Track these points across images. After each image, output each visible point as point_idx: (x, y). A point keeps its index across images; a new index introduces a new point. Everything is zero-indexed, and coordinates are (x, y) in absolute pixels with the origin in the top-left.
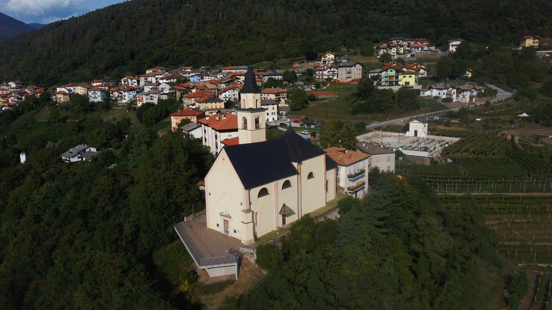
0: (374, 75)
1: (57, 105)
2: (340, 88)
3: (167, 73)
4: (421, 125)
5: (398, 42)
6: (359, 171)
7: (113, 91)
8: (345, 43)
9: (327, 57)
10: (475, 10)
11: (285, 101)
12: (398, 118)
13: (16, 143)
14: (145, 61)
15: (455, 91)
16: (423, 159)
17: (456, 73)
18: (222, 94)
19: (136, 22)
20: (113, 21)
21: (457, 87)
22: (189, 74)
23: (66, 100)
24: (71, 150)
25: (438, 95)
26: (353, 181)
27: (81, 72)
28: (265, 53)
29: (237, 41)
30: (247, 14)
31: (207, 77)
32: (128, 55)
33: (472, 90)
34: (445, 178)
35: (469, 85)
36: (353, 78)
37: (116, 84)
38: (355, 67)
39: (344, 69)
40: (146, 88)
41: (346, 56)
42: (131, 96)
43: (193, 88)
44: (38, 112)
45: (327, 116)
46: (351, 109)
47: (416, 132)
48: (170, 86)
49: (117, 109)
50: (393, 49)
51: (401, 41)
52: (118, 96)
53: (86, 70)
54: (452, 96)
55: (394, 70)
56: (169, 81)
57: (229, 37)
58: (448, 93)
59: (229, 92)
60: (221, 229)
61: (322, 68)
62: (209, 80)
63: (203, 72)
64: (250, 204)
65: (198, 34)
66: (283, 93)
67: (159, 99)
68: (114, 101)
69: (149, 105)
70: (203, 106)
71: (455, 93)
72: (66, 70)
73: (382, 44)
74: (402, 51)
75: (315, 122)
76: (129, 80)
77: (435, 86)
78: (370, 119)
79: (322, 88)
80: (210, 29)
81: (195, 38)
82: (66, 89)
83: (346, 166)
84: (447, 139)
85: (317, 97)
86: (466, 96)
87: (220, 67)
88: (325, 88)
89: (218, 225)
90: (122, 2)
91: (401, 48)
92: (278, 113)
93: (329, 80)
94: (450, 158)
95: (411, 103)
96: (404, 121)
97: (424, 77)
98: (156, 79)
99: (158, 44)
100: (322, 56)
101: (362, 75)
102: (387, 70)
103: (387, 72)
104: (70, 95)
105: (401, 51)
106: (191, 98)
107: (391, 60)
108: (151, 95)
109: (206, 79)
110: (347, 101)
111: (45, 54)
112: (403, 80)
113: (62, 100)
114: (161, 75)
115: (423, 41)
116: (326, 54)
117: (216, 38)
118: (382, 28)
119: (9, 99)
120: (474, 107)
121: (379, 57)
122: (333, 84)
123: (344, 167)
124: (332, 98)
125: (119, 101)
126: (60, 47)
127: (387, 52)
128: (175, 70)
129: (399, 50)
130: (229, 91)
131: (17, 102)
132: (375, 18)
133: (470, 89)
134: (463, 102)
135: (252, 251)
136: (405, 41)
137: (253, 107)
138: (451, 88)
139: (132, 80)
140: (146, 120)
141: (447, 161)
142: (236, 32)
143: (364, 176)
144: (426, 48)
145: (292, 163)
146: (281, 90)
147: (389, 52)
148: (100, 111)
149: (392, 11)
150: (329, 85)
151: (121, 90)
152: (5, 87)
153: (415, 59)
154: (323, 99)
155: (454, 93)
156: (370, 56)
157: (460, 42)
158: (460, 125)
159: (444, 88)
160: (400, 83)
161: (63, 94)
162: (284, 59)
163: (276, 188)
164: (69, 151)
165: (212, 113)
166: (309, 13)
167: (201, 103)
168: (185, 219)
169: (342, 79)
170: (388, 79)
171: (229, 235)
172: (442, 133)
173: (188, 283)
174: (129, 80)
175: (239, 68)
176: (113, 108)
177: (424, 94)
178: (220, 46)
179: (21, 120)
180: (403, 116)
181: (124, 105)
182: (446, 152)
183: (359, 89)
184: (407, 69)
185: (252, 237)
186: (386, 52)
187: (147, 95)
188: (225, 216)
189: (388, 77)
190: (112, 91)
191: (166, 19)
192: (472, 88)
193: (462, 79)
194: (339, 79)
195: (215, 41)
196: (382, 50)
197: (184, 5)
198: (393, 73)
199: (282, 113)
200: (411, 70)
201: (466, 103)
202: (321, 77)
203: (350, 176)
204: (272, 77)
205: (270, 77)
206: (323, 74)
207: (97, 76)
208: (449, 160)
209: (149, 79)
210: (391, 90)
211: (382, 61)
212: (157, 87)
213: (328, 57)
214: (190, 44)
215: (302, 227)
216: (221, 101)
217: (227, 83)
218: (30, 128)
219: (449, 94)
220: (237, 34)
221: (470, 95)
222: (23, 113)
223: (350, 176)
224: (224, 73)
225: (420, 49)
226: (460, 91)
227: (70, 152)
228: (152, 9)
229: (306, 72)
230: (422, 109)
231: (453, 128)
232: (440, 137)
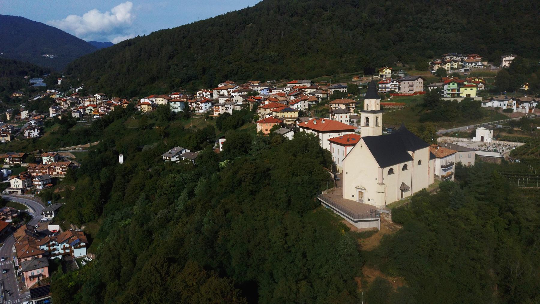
0: (434, 88)
1: (142, 114)
2: (404, 100)
3: (238, 87)
4: (487, 131)
5: (451, 58)
6: (449, 164)
7: (191, 103)
8: (401, 59)
9: (384, 72)
10: (527, 27)
11: (354, 110)
12: (463, 126)
13: (115, 146)
14: (217, 76)
15: (515, 102)
16: (494, 159)
17: (513, 87)
18: (295, 105)
19: (205, 41)
20: (184, 40)
21: (517, 99)
22: (257, 88)
23: (150, 110)
24: (170, 151)
25: (499, 106)
26: (445, 171)
27: (158, 85)
28: (325, 69)
29: (298, 57)
30: (306, 33)
31: (275, 91)
32: (201, 70)
33: (532, 102)
34: (516, 175)
35: (529, 97)
36: (415, 91)
37: (192, 96)
38: (417, 81)
39: (406, 82)
40: (221, 99)
41: (401, 70)
42: (207, 107)
43: (265, 99)
44: (126, 120)
45: (397, 123)
46: (418, 118)
47: (482, 138)
48: (244, 98)
49: (196, 118)
50: (447, 65)
51: (455, 57)
52: (196, 107)
53: (162, 83)
54: (513, 107)
55: (456, 83)
56: (240, 94)
57: (291, 55)
58: (508, 104)
59: (300, 103)
60: (356, 199)
61: (385, 81)
62: (277, 93)
63: (270, 86)
64: (383, 179)
65: (263, 51)
66: (353, 103)
67: (233, 110)
68: (192, 111)
69: (227, 114)
70: (280, 115)
71: (515, 104)
72: (145, 84)
73: (436, 60)
74: (456, 67)
75: (387, 129)
76: (204, 93)
77: (496, 97)
78: (437, 126)
79: (386, 99)
80: (274, 47)
81: (260, 55)
82: (149, 100)
83: (441, 158)
84: (512, 144)
85: (384, 107)
86: (525, 107)
87: (284, 82)
88: (389, 99)
89: (353, 196)
90: (190, 23)
91: (455, 63)
92: (350, 121)
93: (391, 92)
94: (518, 159)
95: (475, 113)
96: (469, 128)
97: (482, 90)
98: (229, 92)
99: (227, 60)
100: (380, 70)
101: (423, 88)
102: (449, 84)
103: (449, 86)
104: (152, 105)
105: (455, 66)
106: (267, 108)
107: (446, 75)
108: (226, 106)
109: (275, 92)
110: (413, 111)
111: (124, 70)
112: (465, 92)
113: (146, 110)
114: (233, 88)
115: (475, 56)
116: (384, 69)
117: (279, 55)
118: (435, 45)
119: (100, 109)
120: (535, 117)
121: (435, 72)
122: (397, 96)
123: (439, 159)
124: (399, 108)
125: (197, 111)
126: (137, 63)
127: (442, 67)
128: (244, 84)
129: (454, 65)
130: (301, 102)
131: (106, 111)
132: (427, 35)
133: (529, 101)
134: (523, 112)
135: (388, 212)
136: (459, 57)
137: (375, 110)
138: (511, 100)
139: (206, 92)
140: (225, 128)
141: (516, 161)
142: (298, 49)
143: (452, 168)
144: (479, 63)
145: (408, 152)
146: (350, 101)
147: (443, 67)
148: (180, 119)
149: (444, 29)
150: (392, 97)
151: (198, 102)
152: (92, 99)
153: (469, 73)
154: (390, 109)
155: (514, 104)
156: (425, 71)
157: (514, 58)
158: (522, 132)
159: (505, 99)
160: (461, 95)
161: (147, 105)
162: (343, 74)
163: (399, 169)
164: (168, 152)
165: (288, 121)
166: (363, 31)
167: (279, 112)
168: (323, 192)
169: (404, 91)
170: (450, 92)
171: (363, 203)
172: (507, 139)
173: (345, 231)
174: (204, 93)
175: (303, 82)
176: (192, 117)
177: (485, 105)
178: (283, 63)
179: (111, 126)
180: (467, 124)
181: (201, 115)
182: (514, 154)
183: (425, 100)
184: (468, 82)
185: (384, 204)
186: (441, 67)
187: (222, 106)
188: (360, 189)
189: (451, 90)
190: (190, 102)
191: (233, 38)
192: (532, 99)
193: (519, 92)
194: (402, 91)
195: (278, 58)
196: (437, 65)
197: (248, 25)
198: (455, 86)
199: (353, 121)
200: (472, 84)
201: (525, 114)
202: (383, 90)
203: (443, 167)
204: (338, 89)
205: (336, 89)
206: (386, 87)
207: (174, 89)
208: (518, 161)
209: (222, 92)
210: (456, 101)
211: (438, 75)
212: (232, 99)
213: (386, 71)
214: (255, 61)
215: (421, 197)
216: (294, 111)
217: (296, 96)
218: (123, 134)
219: (509, 105)
220: (298, 51)
221: (529, 106)
222: (113, 121)
223: (443, 167)
224: (289, 86)
225: (474, 64)
226: (519, 102)
227: (169, 153)
228: (219, 29)
229: (367, 85)
230: (484, 118)
231: (516, 135)
232: (505, 142)
